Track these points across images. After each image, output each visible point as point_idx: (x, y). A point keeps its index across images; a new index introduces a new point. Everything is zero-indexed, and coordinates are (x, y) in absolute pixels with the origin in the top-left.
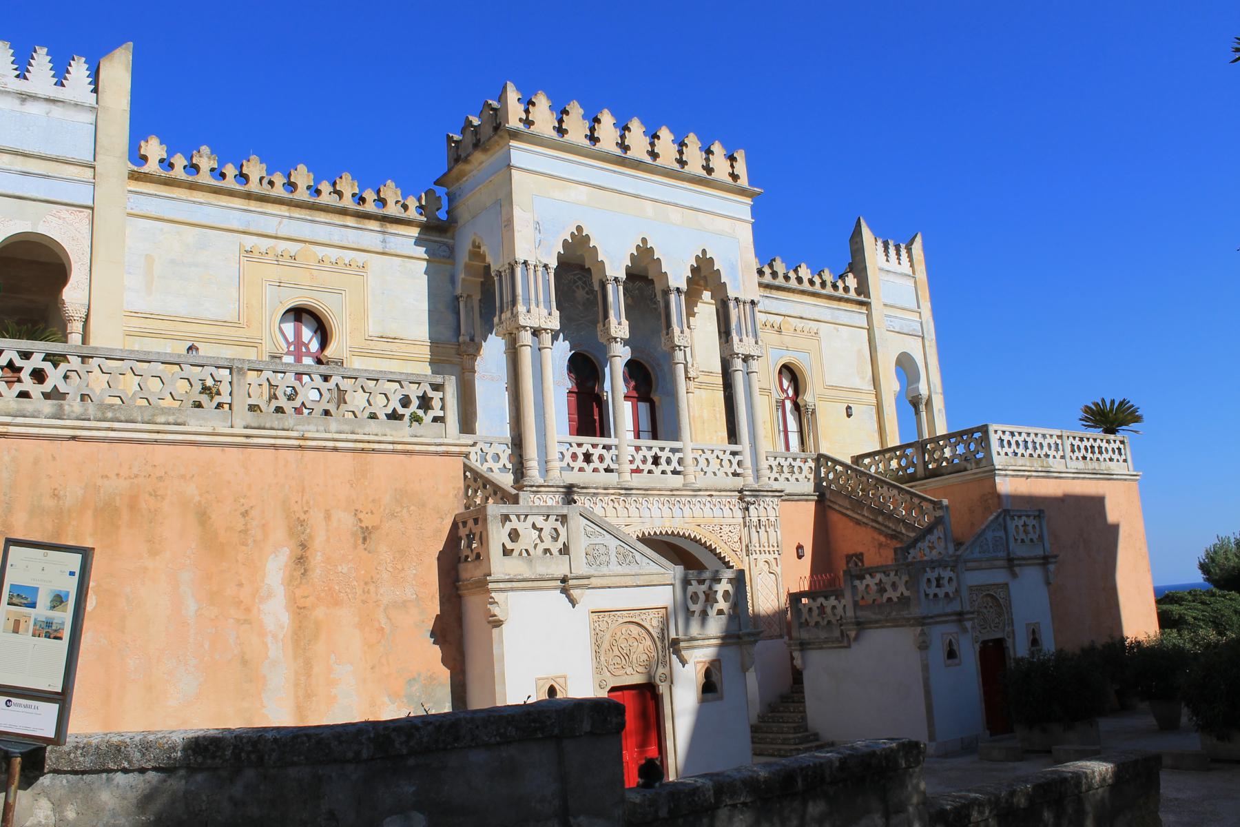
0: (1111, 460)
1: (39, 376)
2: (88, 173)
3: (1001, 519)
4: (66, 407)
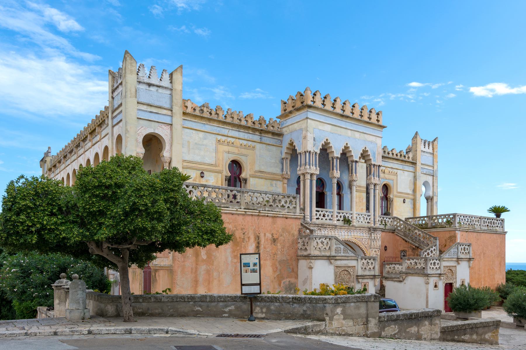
0: (497, 226)
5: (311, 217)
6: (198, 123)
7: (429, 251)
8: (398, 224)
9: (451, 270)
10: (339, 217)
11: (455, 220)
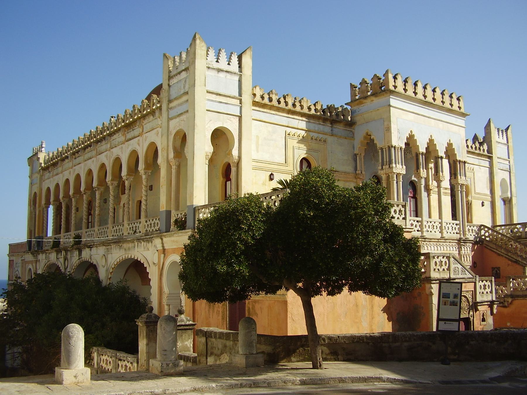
6: (277, 115)
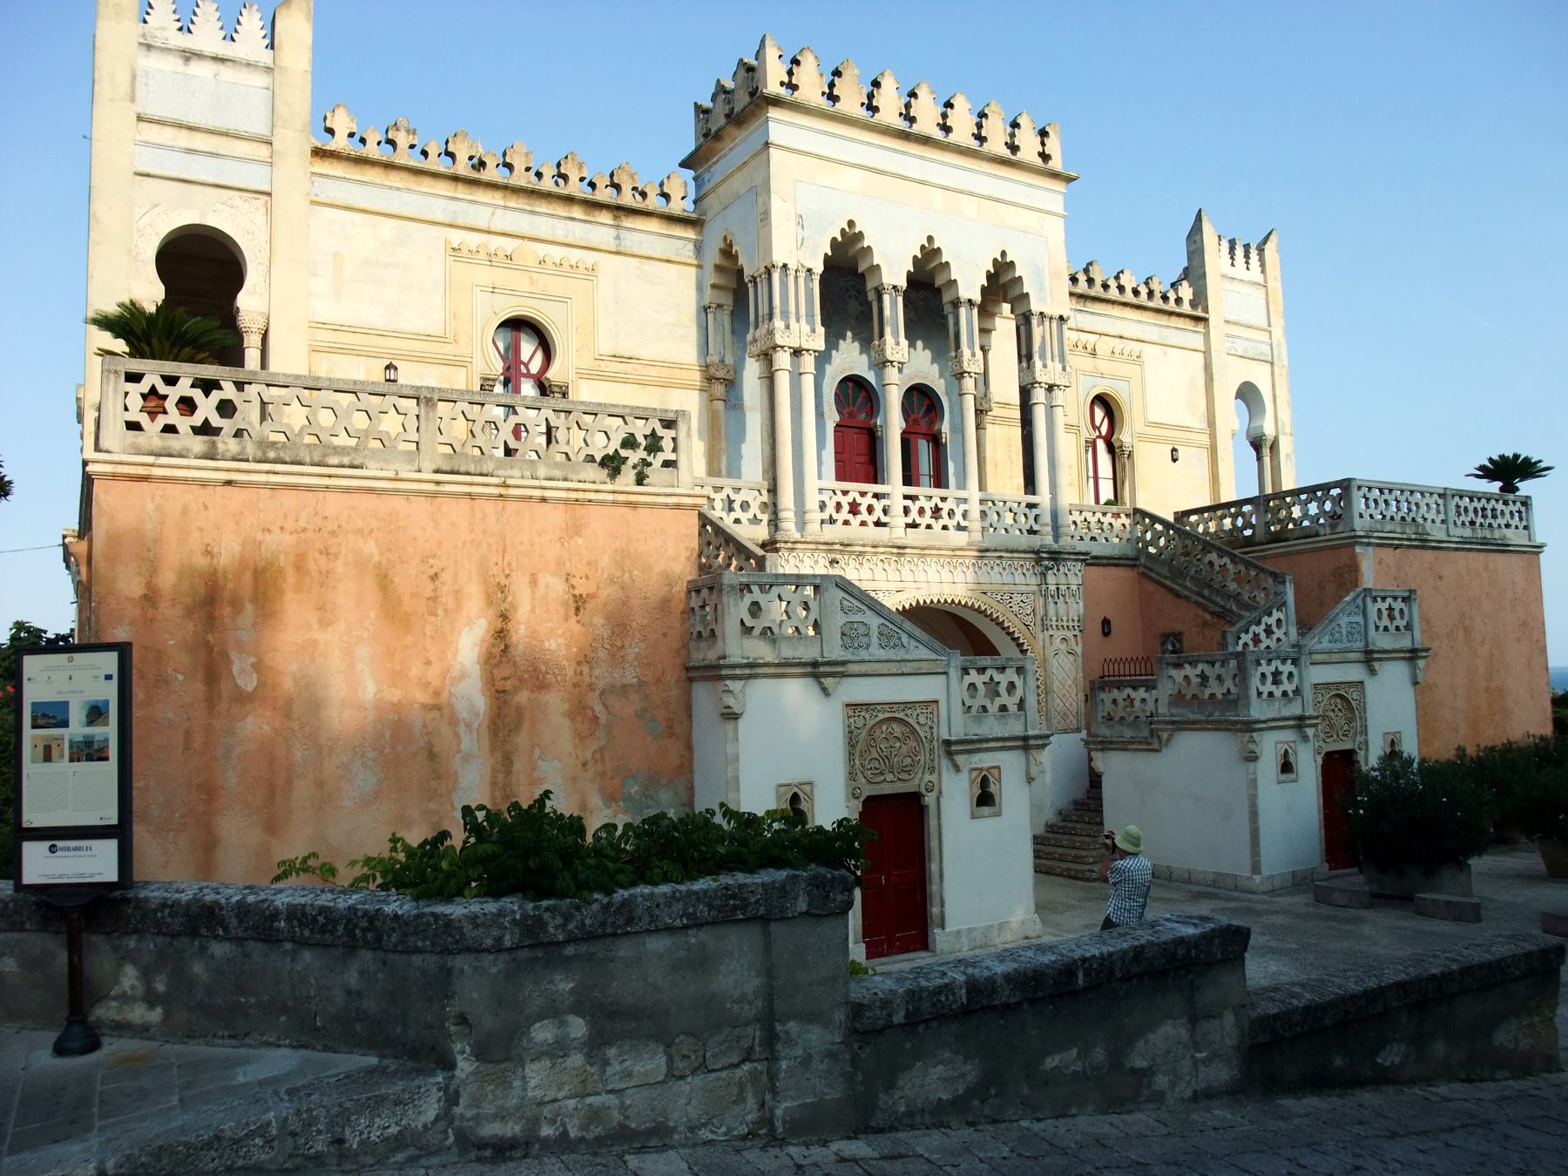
0: (1508, 526)
1: (187, 405)
2: (263, 151)
3: (1359, 601)
4: (220, 446)
5: (801, 513)
7: (1260, 629)
8: (1149, 536)
9: (1347, 702)
10: (914, 514)
11: (1349, 504)
